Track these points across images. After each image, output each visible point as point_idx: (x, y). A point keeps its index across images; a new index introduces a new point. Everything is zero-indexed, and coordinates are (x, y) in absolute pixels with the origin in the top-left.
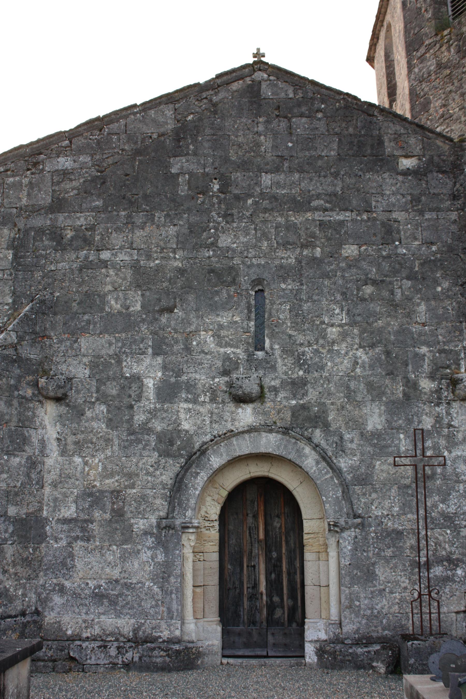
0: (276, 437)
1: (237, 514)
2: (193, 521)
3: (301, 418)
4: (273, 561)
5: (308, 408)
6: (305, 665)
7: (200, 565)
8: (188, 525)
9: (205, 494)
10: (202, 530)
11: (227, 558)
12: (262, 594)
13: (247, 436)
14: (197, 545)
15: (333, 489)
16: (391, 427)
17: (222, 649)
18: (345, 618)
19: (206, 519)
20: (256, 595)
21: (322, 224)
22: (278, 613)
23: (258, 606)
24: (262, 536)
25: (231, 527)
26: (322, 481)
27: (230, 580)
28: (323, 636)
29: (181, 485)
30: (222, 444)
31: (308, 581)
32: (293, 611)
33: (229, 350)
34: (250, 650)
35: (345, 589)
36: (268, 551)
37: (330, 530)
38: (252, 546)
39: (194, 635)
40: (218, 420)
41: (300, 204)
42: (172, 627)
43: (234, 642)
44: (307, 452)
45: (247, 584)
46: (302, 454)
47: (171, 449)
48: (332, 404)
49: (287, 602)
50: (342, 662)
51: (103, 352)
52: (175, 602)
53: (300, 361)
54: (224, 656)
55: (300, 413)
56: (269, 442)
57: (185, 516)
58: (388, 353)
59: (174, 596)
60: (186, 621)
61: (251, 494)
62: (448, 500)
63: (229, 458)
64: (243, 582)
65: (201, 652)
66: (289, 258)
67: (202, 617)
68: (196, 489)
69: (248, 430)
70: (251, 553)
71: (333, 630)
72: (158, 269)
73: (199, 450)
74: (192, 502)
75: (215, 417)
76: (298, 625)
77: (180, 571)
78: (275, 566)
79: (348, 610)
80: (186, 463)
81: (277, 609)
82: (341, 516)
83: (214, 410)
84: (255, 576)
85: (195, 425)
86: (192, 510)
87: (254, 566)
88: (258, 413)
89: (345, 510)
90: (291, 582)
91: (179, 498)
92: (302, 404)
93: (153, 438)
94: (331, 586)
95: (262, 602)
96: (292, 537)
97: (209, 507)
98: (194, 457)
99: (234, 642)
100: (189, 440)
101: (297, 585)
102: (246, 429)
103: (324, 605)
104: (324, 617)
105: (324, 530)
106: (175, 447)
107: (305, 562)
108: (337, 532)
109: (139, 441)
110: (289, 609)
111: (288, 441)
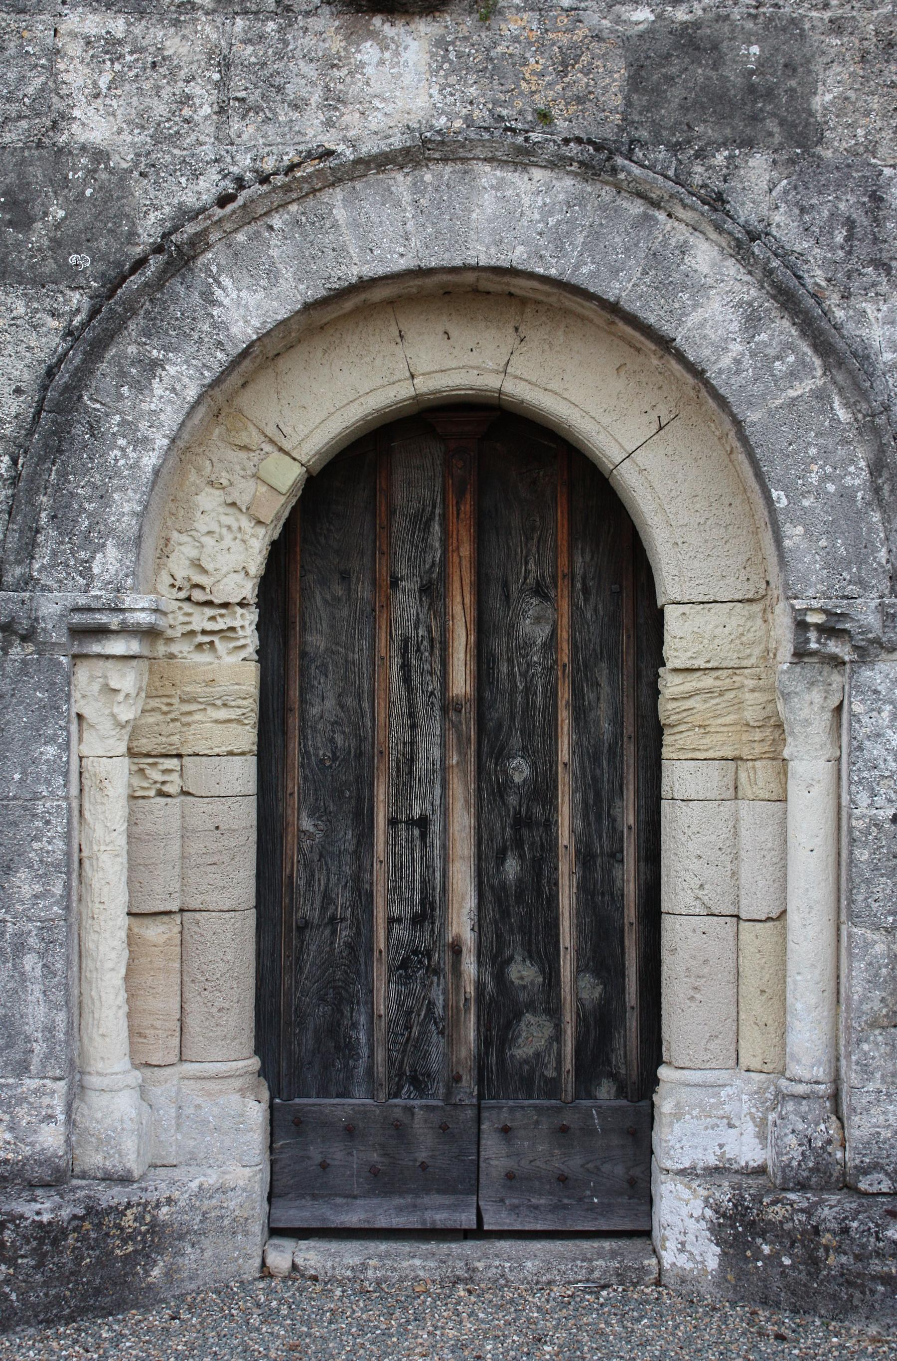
0: (549, 188)
1: (345, 577)
2: (128, 601)
3: (675, 94)
4: (512, 800)
5: (715, 47)
6: (658, 1283)
7: (165, 815)
8: (103, 618)
9: (193, 477)
10: (175, 648)
11: (294, 782)
12: (456, 950)
13: (400, 182)
14: (151, 719)
15: (825, 452)
17: (271, 1197)
18: (866, 1071)
19: (198, 595)
20: (429, 954)
22: (531, 1037)
23: (440, 1002)
24: (461, 682)
25: (317, 641)
26: (771, 414)
27: (309, 884)
28: (748, 1151)
29: (70, 424)
30: (277, 221)
31: (679, 891)
32: (599, 1025)
34: (398, 1201)
35: (869, 935)
36: (490, 749)
37: (800, 654)
38: (413, 727)
39: (130, 1145)
40: (254, 97)
42: (21, 1111)
43: (324, 1166)
44: (704, 268)
45: (389, 902)
46: (676, 277)
47: (18, 245)
48: (837, 27)
49: (575, 986)
50: (849, 1283)
52: (36, 991)
54: (275, 1232)
55: (674, 70)
56: (511, 216)
57: (86, 573)
59: (30, 962)
60: (93, 1081)
61: (415, 484)
63: (315, 293)
64: (370, 896)
65: (165, 1225)
67: (173, 1058)
68: (142, 443)
69: (406, 151)
70: (411, 760)
71: (801, 1126)
73: (158, 249)
74: (125, 506)
75: (239, 85)
76: (621, 1092)
77: (60, 844)
78: (521, 822)
79: (878, 1036)
80: (94, 312)
81: (528, 1017)
82: (860, 582)
83: (238, 48)
84: (429, 866)
85: (141, 121)
86: (121, 545)
87: (423, 823)
88: (461, 67)
89: (883, 555)
90: (597, 899)
91: (58, 489)
92: (685, 25)
94: (794, 919)
95: (457, 987)
96: (605, 689)
97: (208, 541)
98: (136, 287)
99: (324, 1166)
101: (621, 909)
102: (397, 141)
103: (755, 1007)
104: (756, 1064)
105: (769, 655)
106: (39, 235)
107: (666, 806)
108: (837, 662)
110: (582, 1019)
111: (610, 211)
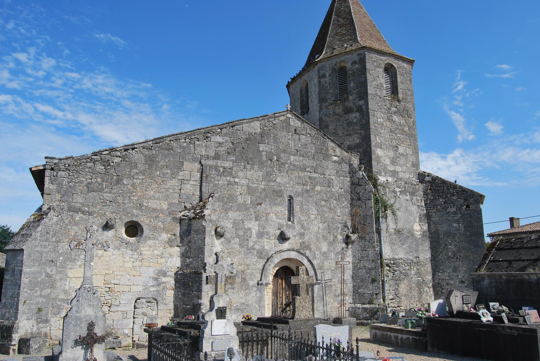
16: (330, 251)
21: (310, 177)
33: (280, 221)
41: (304, 169)
51: (237, 218)
53: (303, 227)
58: (329, 225)
62: (231, 313)
66: (299, 188)
72: (256, 188)
93: (255, 251)
100: (267, 254)
109: (251, 253)
